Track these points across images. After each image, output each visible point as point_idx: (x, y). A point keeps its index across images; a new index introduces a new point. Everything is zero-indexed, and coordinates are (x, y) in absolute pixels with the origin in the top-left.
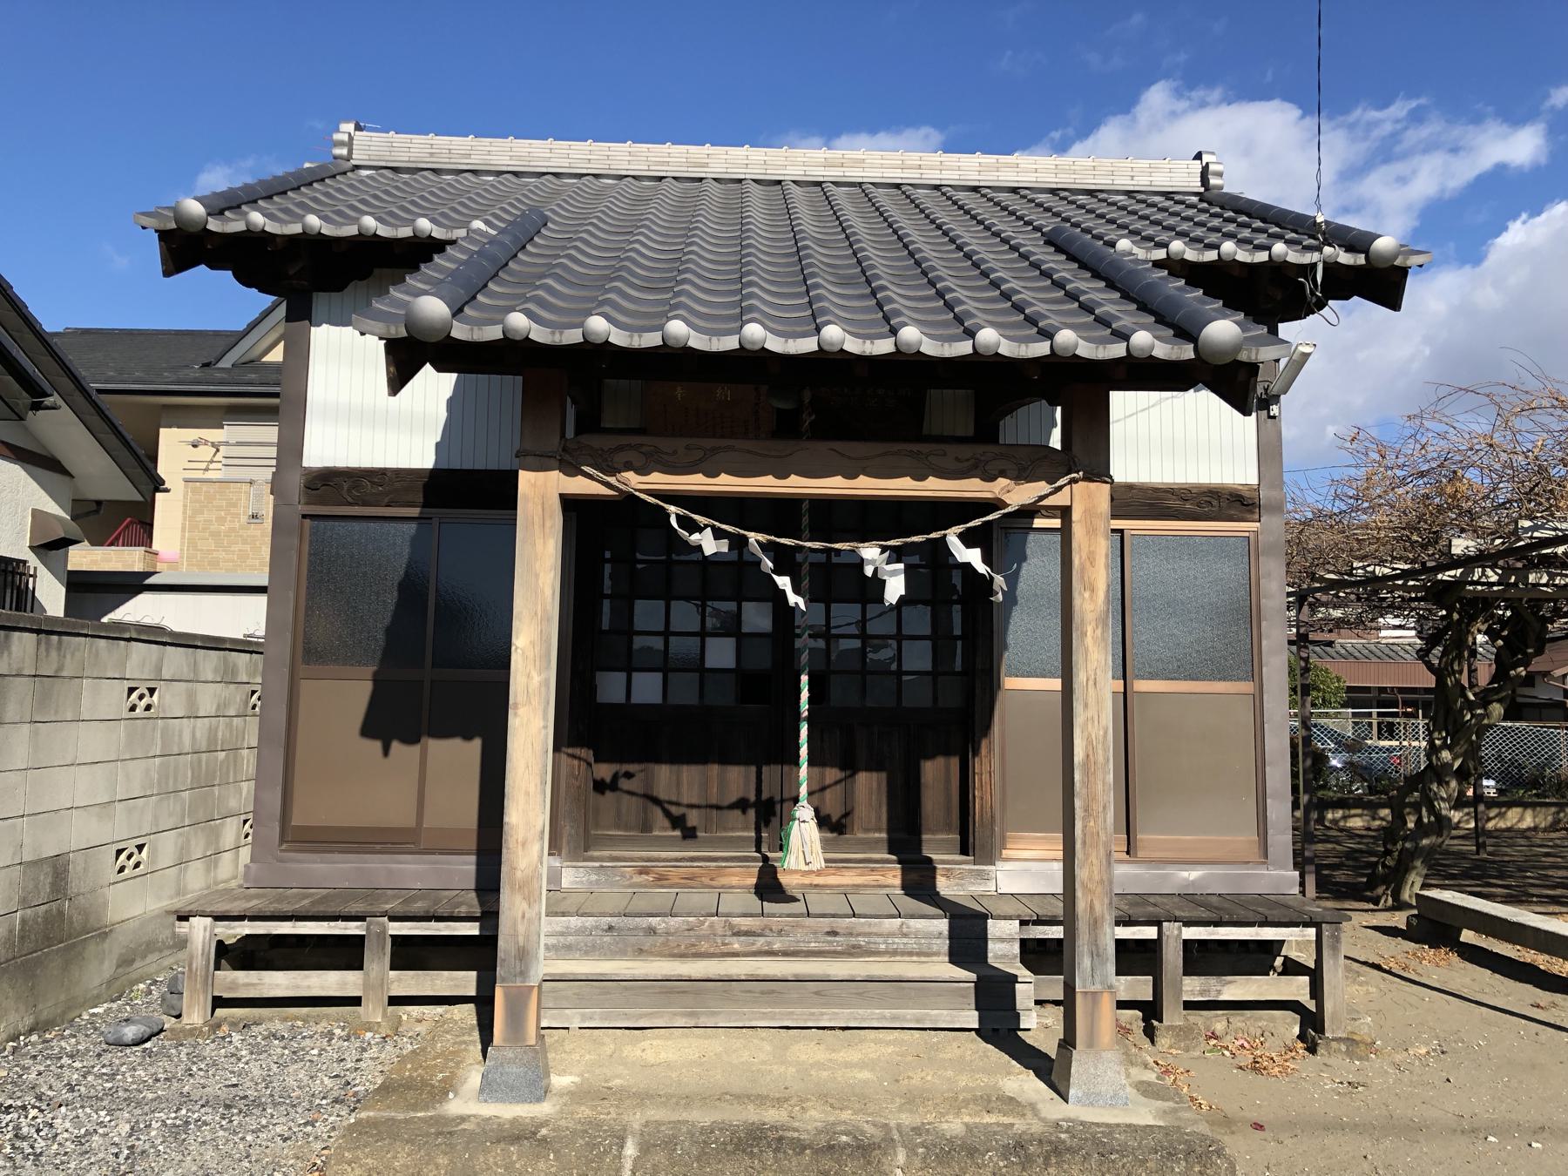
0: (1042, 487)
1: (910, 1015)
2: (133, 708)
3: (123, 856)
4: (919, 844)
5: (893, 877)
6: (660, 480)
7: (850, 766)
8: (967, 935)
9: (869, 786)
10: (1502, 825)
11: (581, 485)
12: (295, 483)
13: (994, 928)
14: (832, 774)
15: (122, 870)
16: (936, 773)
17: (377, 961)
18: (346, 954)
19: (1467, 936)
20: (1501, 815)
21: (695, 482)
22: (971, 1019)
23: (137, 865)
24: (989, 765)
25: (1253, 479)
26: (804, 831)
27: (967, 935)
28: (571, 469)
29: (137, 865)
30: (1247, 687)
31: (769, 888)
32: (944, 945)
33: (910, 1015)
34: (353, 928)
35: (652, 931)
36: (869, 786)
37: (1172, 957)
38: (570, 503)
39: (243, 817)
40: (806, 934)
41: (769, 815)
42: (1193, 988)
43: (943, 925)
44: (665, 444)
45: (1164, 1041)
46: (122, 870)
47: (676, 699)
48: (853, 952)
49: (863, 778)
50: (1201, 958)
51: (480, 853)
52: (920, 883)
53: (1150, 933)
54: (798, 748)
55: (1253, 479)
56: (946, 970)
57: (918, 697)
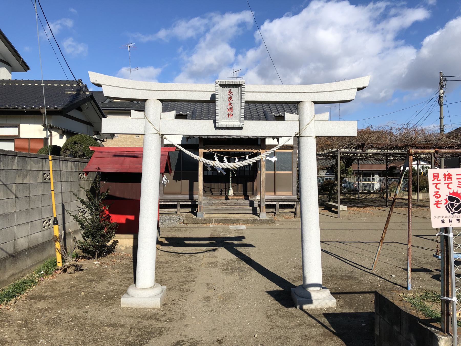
0: (258, 150)
1: (244, 212)
2: (45, 179)
3: (45, 223)
4: (247, 193)
5: (243, 198)
6: (214, 150)
7: (238, 184)
8: (252, 204)
9: (240, 186)
10: (370, 197)
11: (205, 151)
12: (163, 146)
13: (255, 202)
14: (235, 184)
15: (44, 227)
16: (249, 184)
17: (179, 207)
18: (175, 206)
19: (333, 209)
20: (370, 195)
21: (219, 150)
22: (252, 212)
23: (49, 225)
24: (256, 183)
25: (293, 144)
26: (231, 192)
27: (252, 204)
28: (205, 149)
29: (49, 225)
30: (291, 172)
31: (227, 198)
32: (249, 205)
33: (244, 212)
34: (176, 203)
35: (213, 203)
36: (240, 186)
37: (278, 206)
38: (204, 153)
39: (42, 220)
40: (232, 203)
41: (227, 189)
42: (281, 210)
43: (249, 202)
44: (215, 146)
45: (276, 216)
46: (44, 227)
47: (214, 175)
48: (237, 205)
49: (239, 185)
50: (281, 206)
51: (189, 195)
52: (247, 198)
53: (275, 203)
54: (186, 153)
55: (293, 144)
56: (249, 207)
57: (247, 174)
